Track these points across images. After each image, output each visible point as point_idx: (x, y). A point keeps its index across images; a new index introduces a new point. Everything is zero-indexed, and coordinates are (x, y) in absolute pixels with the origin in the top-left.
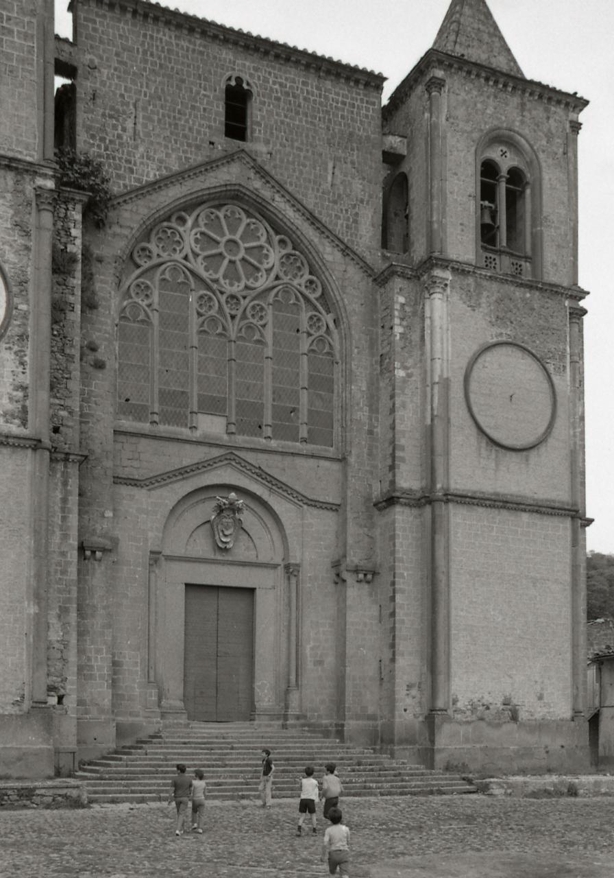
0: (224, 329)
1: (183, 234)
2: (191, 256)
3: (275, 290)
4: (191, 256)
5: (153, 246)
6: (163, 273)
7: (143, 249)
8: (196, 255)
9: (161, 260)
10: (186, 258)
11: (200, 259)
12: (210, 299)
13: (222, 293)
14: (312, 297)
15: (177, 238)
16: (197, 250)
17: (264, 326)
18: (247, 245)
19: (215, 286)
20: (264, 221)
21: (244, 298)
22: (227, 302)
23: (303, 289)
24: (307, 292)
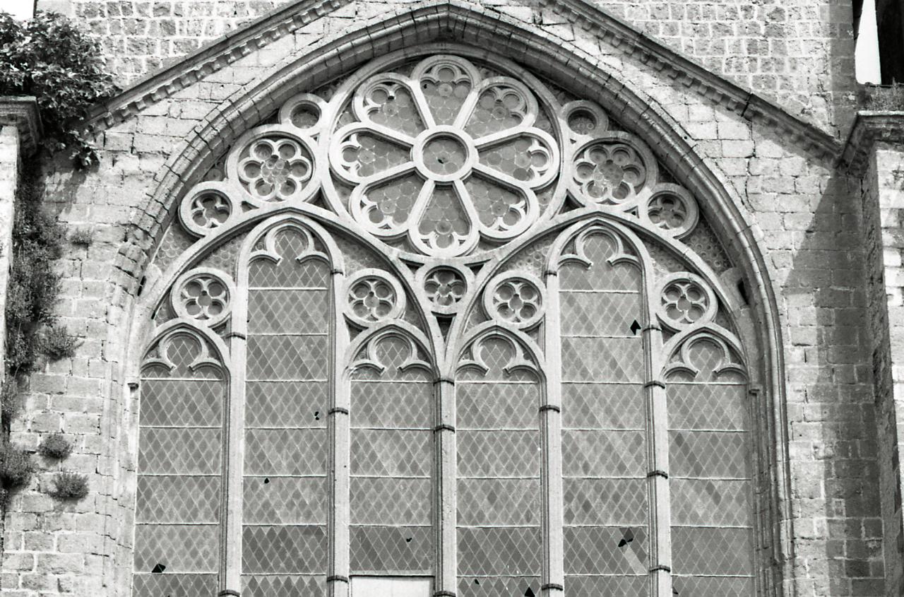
0: (422, 352)
1: (311, 144)
2: (332, 194)
3: (564, 237)
4: (332, 194)
5: (230, 187)
6: (260, 243)
7: (208, 197)
8: (345, 187)
9: (566, 142)
10: (320, 199)
11: (357, 195)
12: (384, 286)
13: (414, 266)
14: (670, 234)
15: (298, 155)
16: (352, 176)
17: (534, 330)
18: (484, 140)
19: (394, 253)
20: (528, 77)
21: (476, 268)
22: (430, 287)
23: (644, 221)
24: (654, 228)
